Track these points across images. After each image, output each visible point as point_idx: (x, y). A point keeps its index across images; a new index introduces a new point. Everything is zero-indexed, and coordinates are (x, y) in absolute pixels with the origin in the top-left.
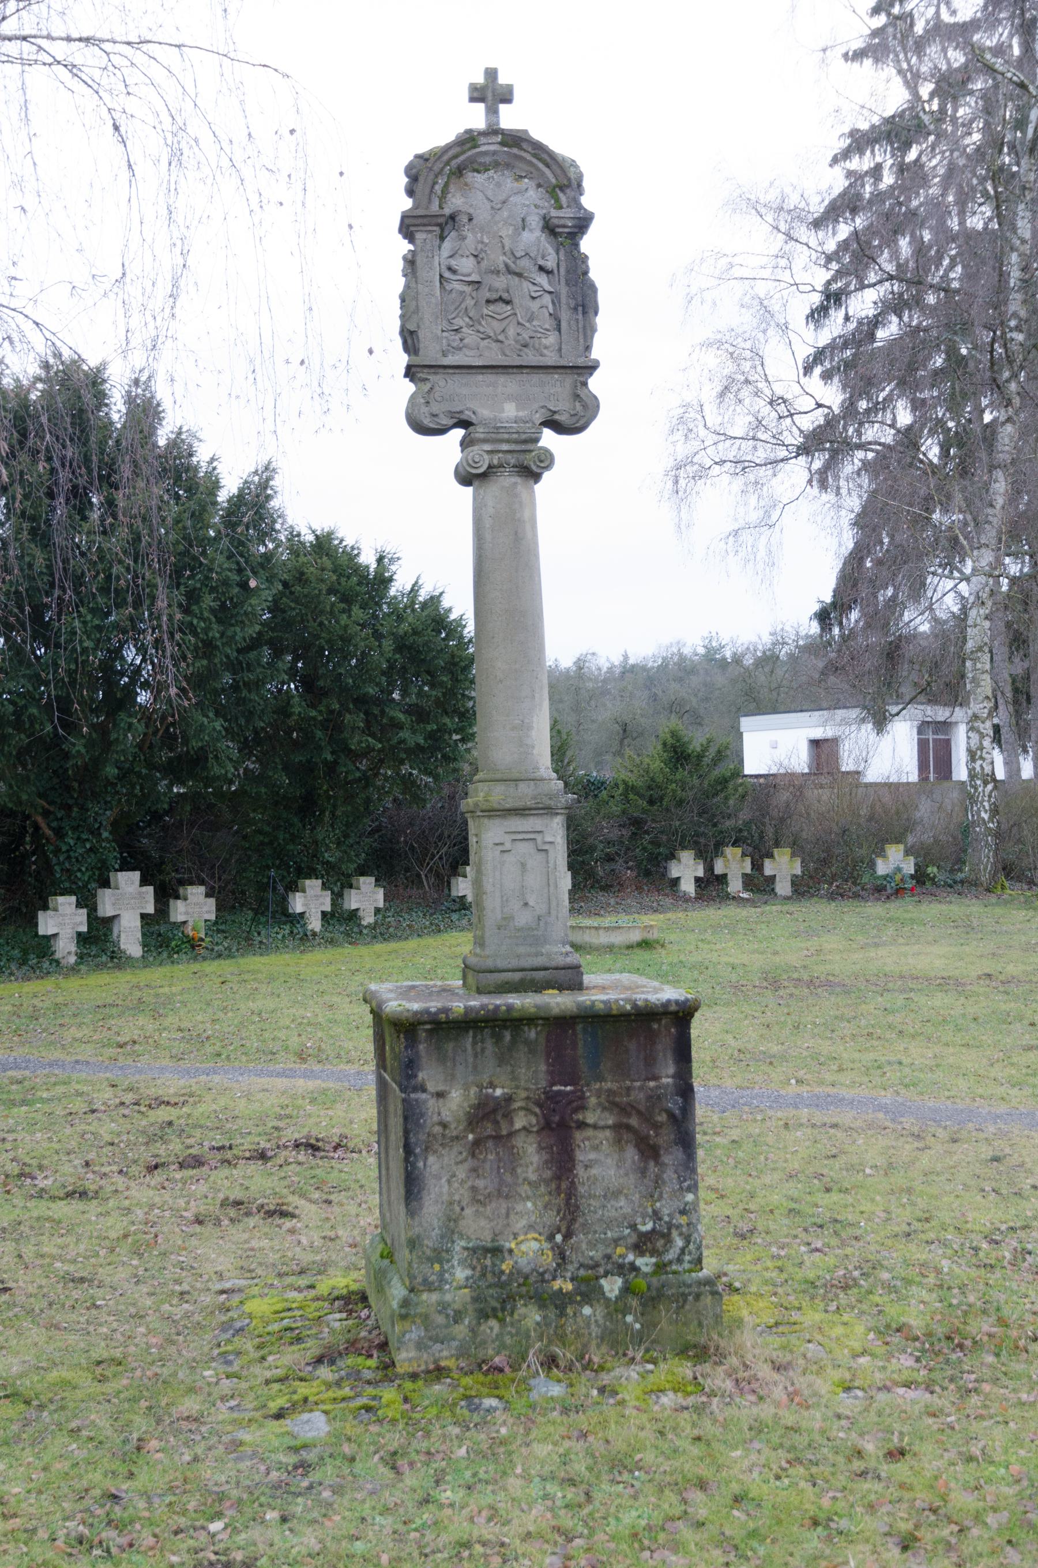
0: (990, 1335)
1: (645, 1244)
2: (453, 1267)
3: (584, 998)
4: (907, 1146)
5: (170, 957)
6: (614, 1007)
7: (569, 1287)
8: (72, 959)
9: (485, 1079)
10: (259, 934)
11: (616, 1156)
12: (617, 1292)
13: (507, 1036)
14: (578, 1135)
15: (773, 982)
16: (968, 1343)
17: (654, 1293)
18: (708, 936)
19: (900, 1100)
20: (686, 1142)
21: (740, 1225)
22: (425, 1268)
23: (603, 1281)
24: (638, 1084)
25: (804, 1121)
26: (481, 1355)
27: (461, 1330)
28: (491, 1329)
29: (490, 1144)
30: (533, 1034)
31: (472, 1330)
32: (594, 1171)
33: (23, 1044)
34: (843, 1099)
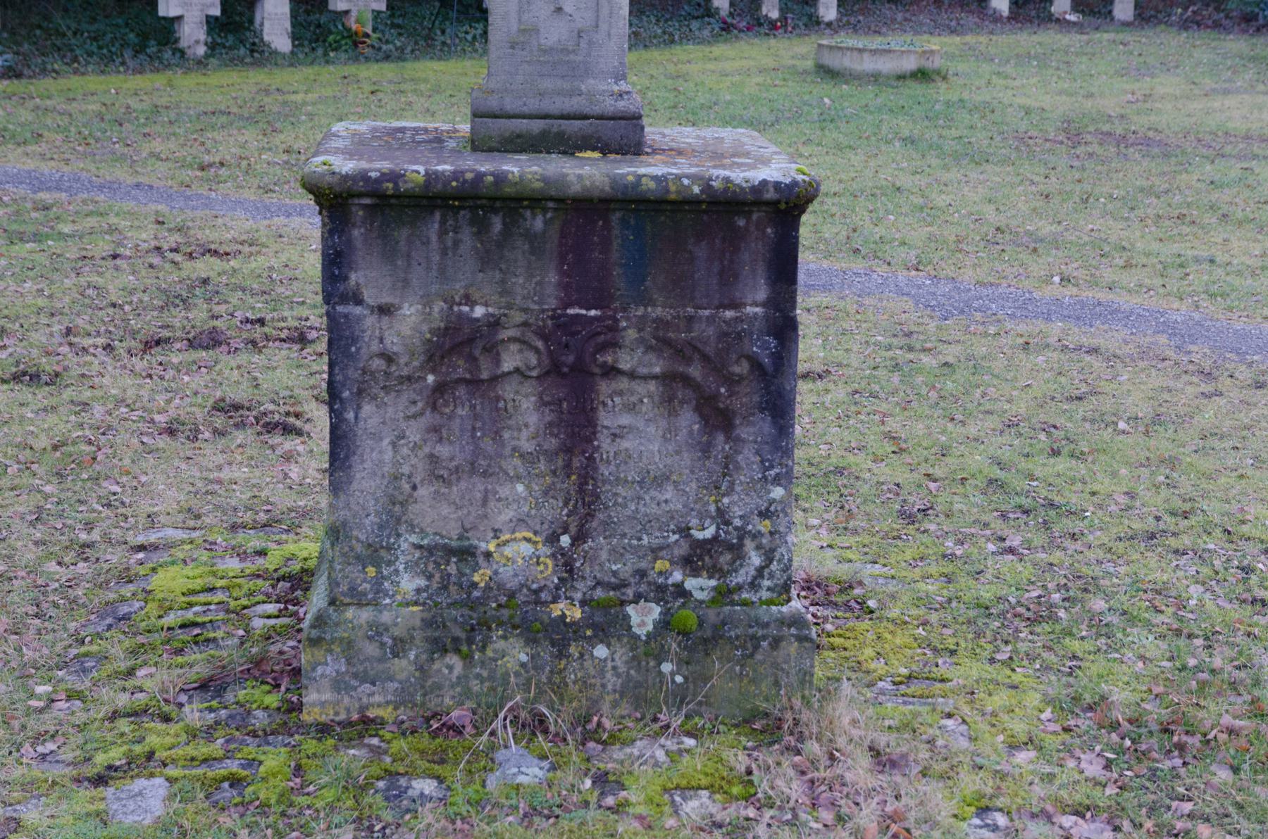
0: (1231, 731)
1: (701, 558)
2: (397, 571)
3: (647, 171)
4: (1190, 390)
5: (326, 54)
6: (673, 188)
7: (577, 613)
8: (201, 50)
9: (458, 288)
10: (443, 32)
11: (663, 423)
12: (650, 628)
13: (497, 224)
14: (604, 387)
15: (1073, 134)
16: (1194, 741)
17: (709, 633)
18: (1009, 69)
19: (1197, 316)
20: (779, 408)
21: (911, 499)
22: (354, 572)
23: (630, 610)
24: (707, 312)
25: (1052, 341)
26: (433, 703)
27: (403, 667)
28: (450, 668)
29: (461, 391)
30: (539, 224)
31: (421, 669)
32: (625, 444)
33: (84, 155)
34: (1117, 311)
